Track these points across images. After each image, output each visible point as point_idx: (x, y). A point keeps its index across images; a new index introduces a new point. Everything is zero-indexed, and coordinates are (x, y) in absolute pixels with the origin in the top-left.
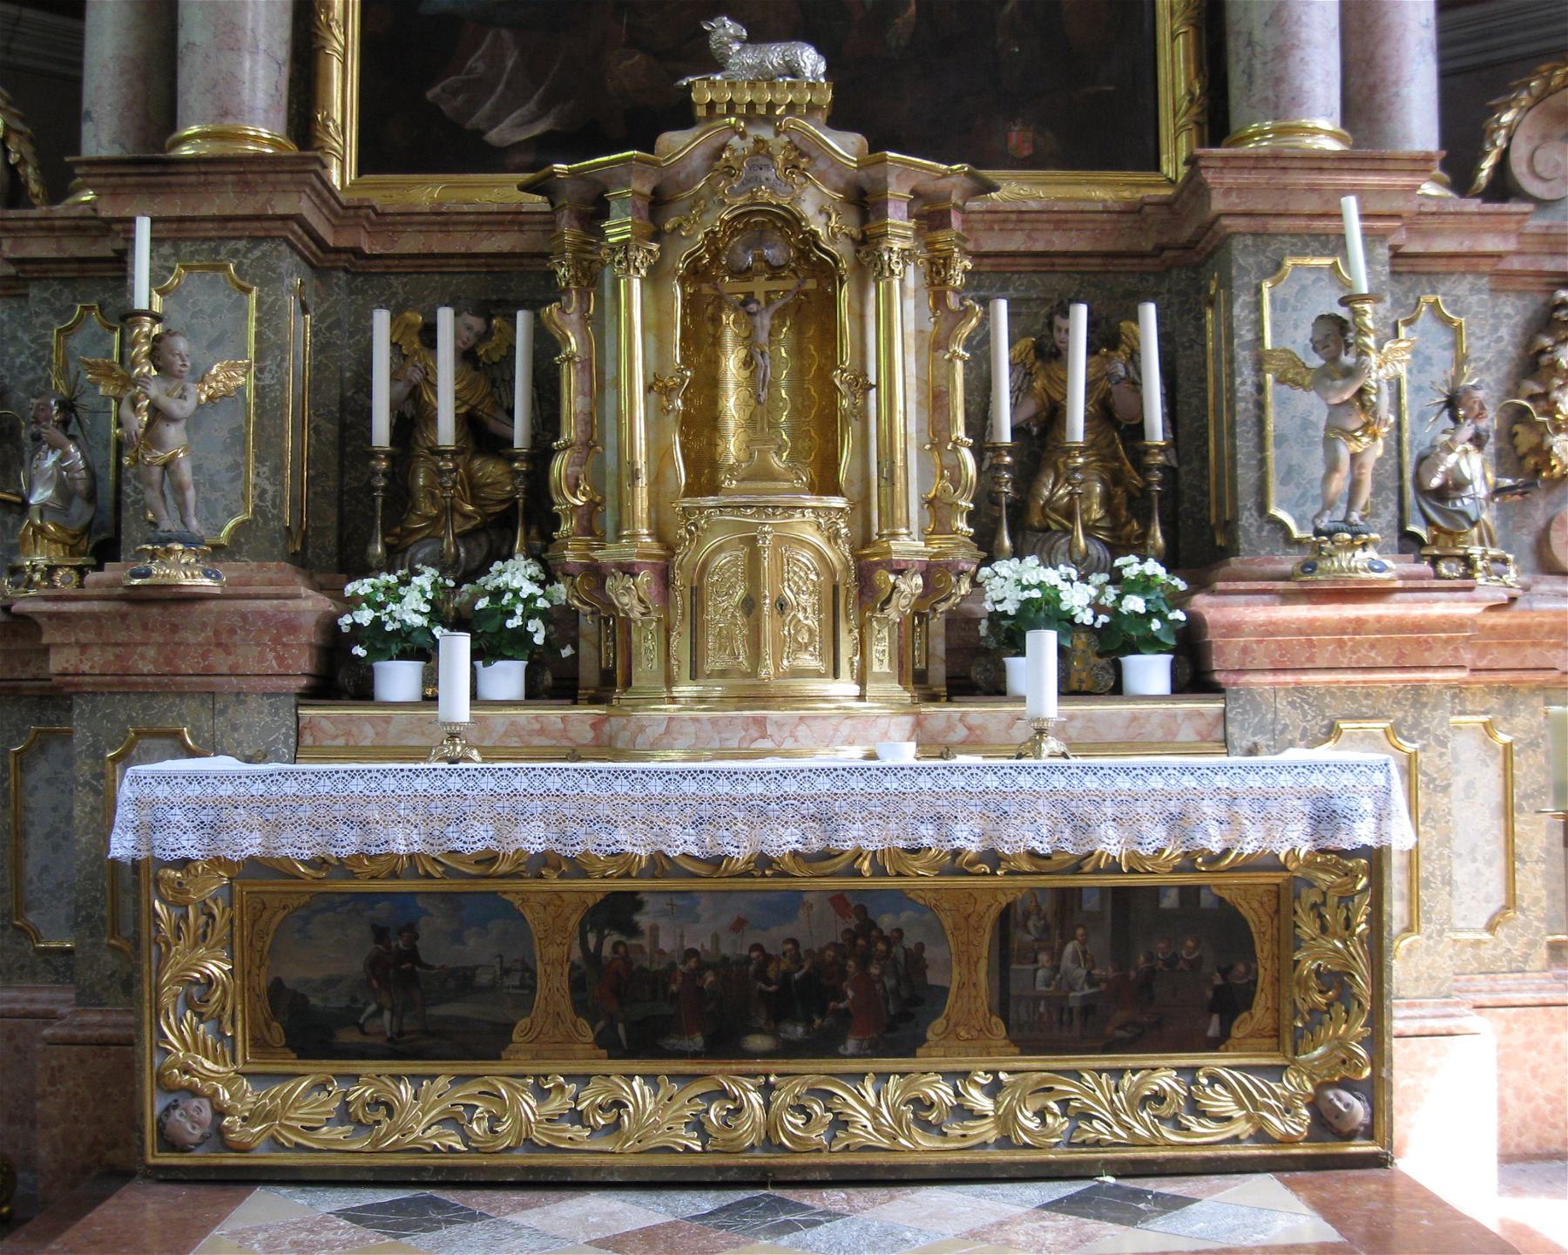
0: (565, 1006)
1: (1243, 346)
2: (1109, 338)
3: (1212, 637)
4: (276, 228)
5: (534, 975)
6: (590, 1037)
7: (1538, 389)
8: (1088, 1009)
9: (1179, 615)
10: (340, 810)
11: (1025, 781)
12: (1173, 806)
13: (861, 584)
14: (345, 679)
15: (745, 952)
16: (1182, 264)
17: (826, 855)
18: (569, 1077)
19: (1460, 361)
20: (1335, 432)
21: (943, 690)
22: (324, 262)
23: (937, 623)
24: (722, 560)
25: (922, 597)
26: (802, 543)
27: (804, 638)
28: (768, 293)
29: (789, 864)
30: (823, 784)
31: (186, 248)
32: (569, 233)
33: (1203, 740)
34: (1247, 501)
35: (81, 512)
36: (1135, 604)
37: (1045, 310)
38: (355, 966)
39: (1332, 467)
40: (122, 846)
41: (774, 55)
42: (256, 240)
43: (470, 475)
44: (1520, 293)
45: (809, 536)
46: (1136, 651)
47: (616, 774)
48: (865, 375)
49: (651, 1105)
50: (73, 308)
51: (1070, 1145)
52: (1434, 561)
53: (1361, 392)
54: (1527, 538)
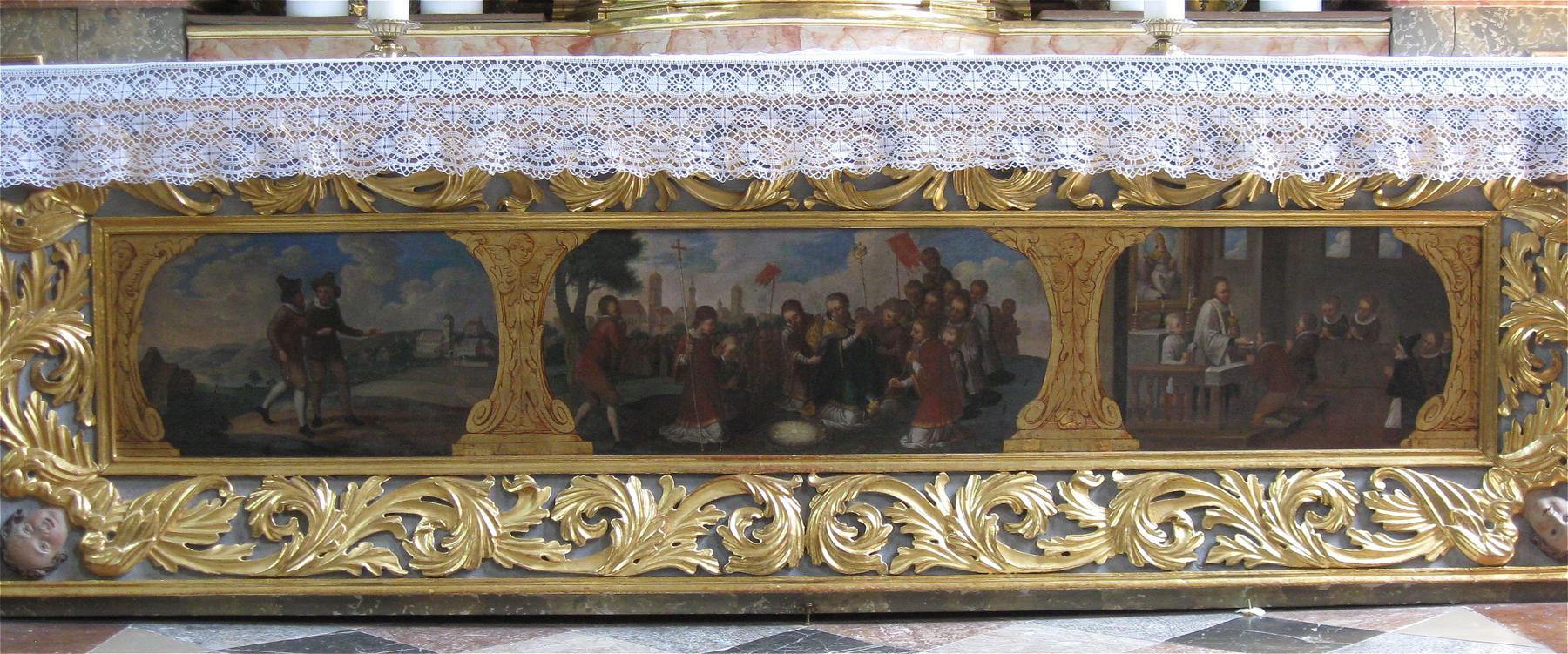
0: (536, 383)
5: (494, 341)
8: (1230, 390)
15: (777, 310)
17: (885, 180)
18: (542, 478)
38: (257, 331)
51: (1206, 566)
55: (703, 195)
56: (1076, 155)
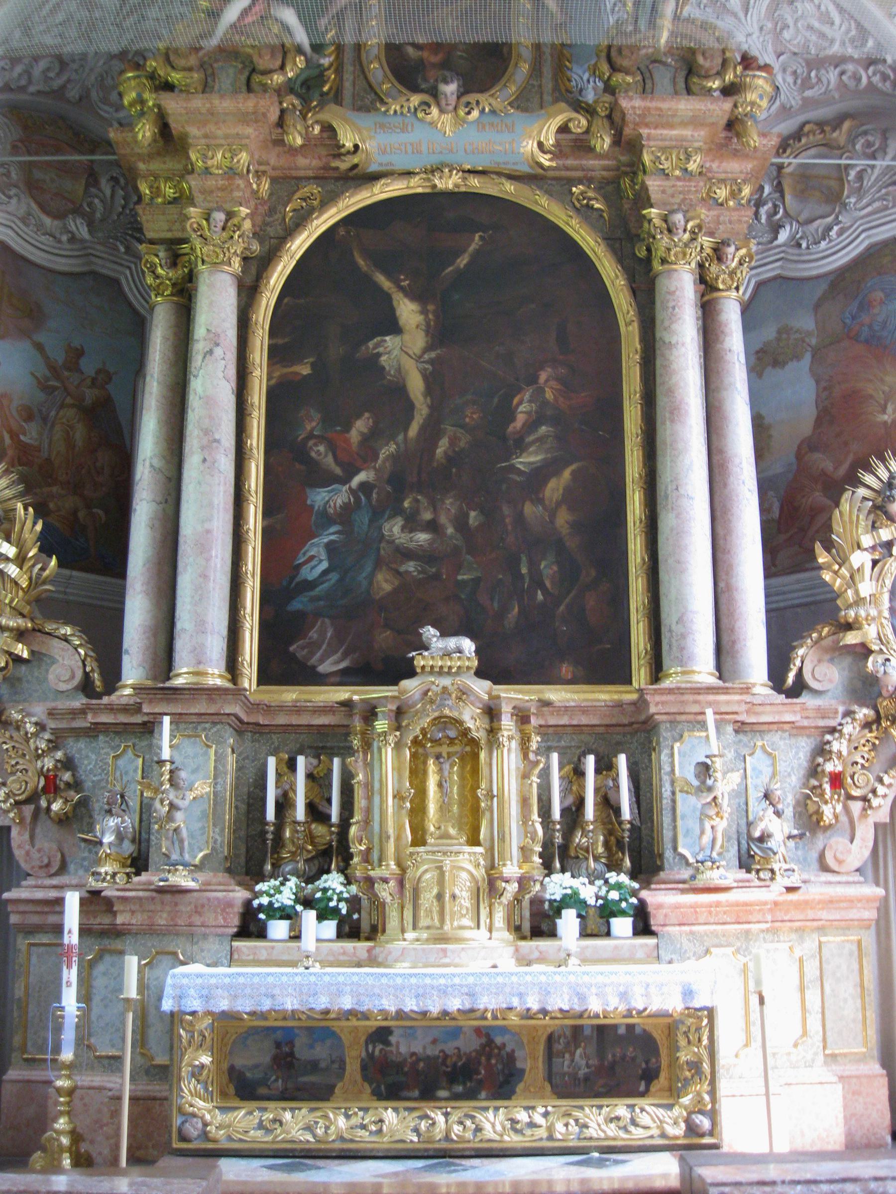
0: (359, 1078)
1: (666, 774)
2: (605, 766)
3: (650, 909)
4: (225, 719)
5: (345, 1063)
6: (369, 1090)
7: (816, 783)
8: (587, 1079)
9: (634, 900)
10: (263, 990)
11: (558, 978)
12: (622, 989)
13: (491, 886)
14: (253, 928)
15: (437, 1053)
16: (636, 735)
17: (472, 1011)
18: (360, 1109)
19: (774, 775)
20: (703, 816)
21: (529, 934)
22: (242, 728)
23: (526, 903)
24: (428, 876)
25: (519, 891)
26: (463, 869)
27: (464, 912)
28: (448, 753)
29: (456, 1014)
30: (471, 980)
31: (182, 726)
32: (357, 724)
33: (648, 957)
34: (668, 845)
35: (128, 848)
36: (614, 895)
37: (578, 752)
38: (267, 1059)
39: (702, 832)
40: (167, 1005)
41: (452, 642)
42: (214, 723)
43: (310, 832)
44: (808, 736)
45: (466, 864)
46: (615, 916)
47: (382, 975)
48: (491, 790)
49: (395, 1121)
50: (119, 746)
51: (579, 1139)
52: (758, 871)
53: (715, 798)
54: (814, 855)
55: (413, 1015)
56: (534, 1005)
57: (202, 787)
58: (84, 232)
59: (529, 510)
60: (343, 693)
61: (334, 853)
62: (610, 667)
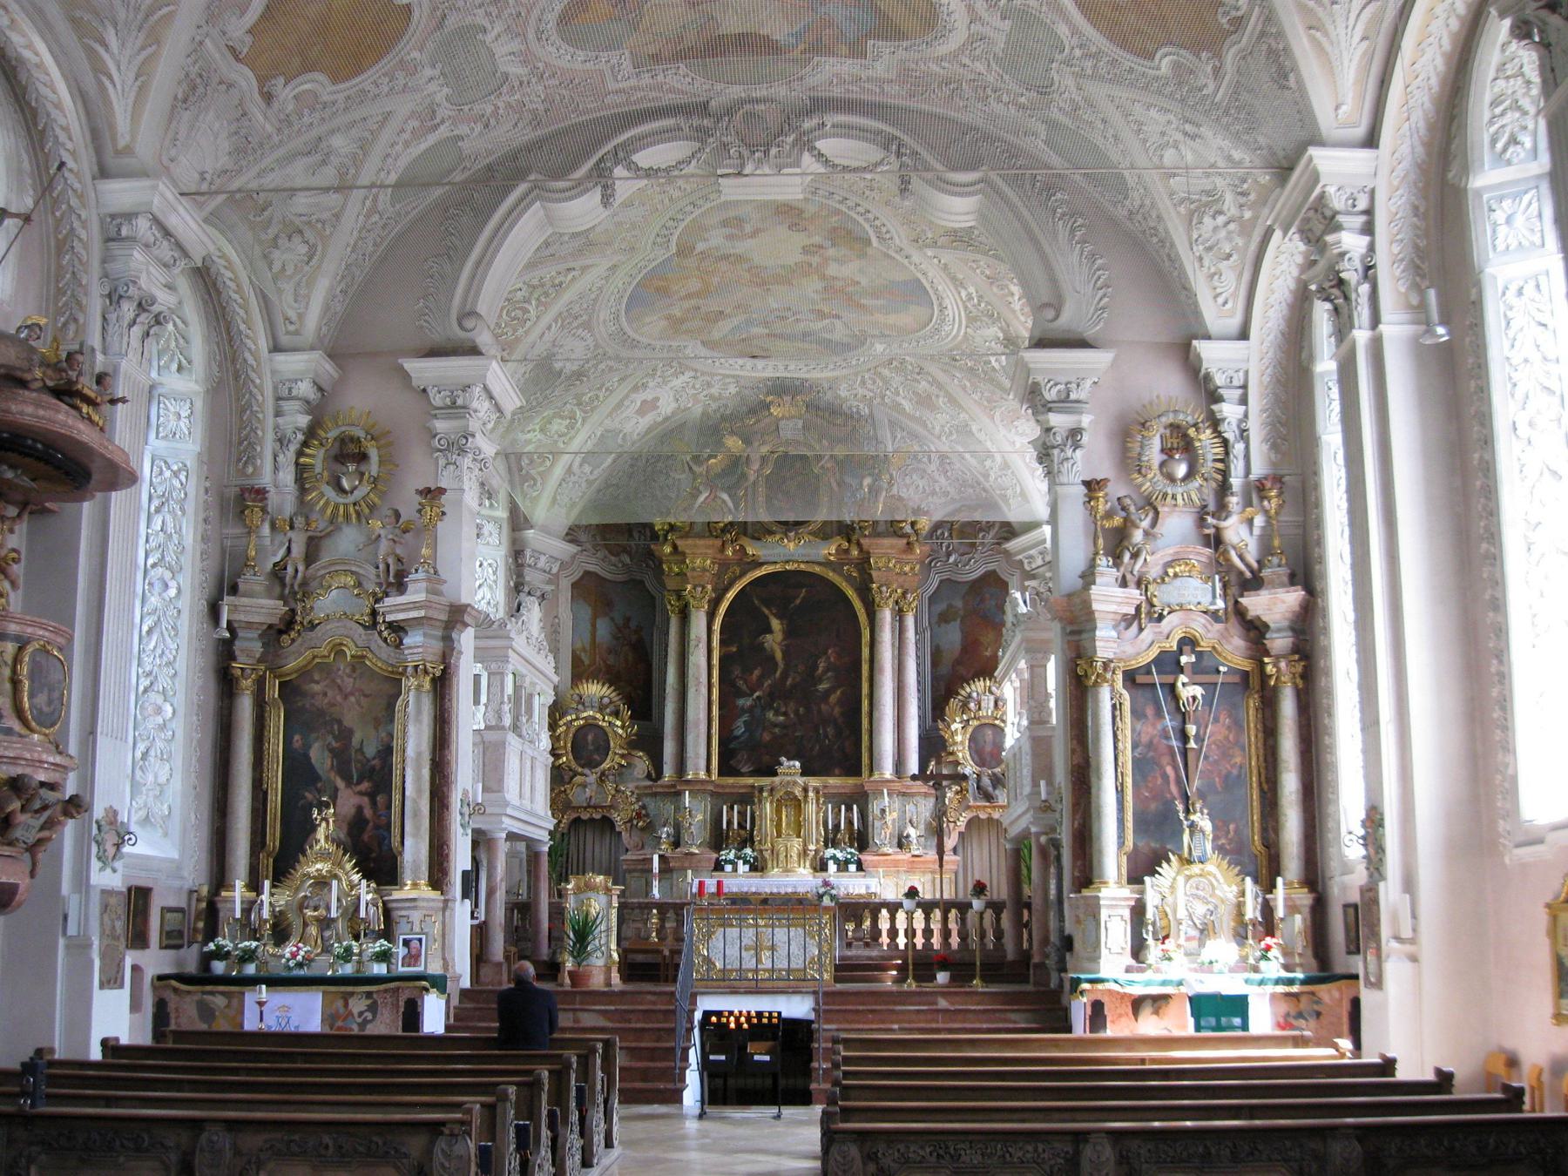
2: (849, 809)
13: (804, 853)
16: (860, 798)
22: (713, 794)
45: (796, 844)
57: (700, 817)
58: (627, 560)
59: (824, 707)
60: (750, 781)
61: (749, 840)
62: (853, 769)
